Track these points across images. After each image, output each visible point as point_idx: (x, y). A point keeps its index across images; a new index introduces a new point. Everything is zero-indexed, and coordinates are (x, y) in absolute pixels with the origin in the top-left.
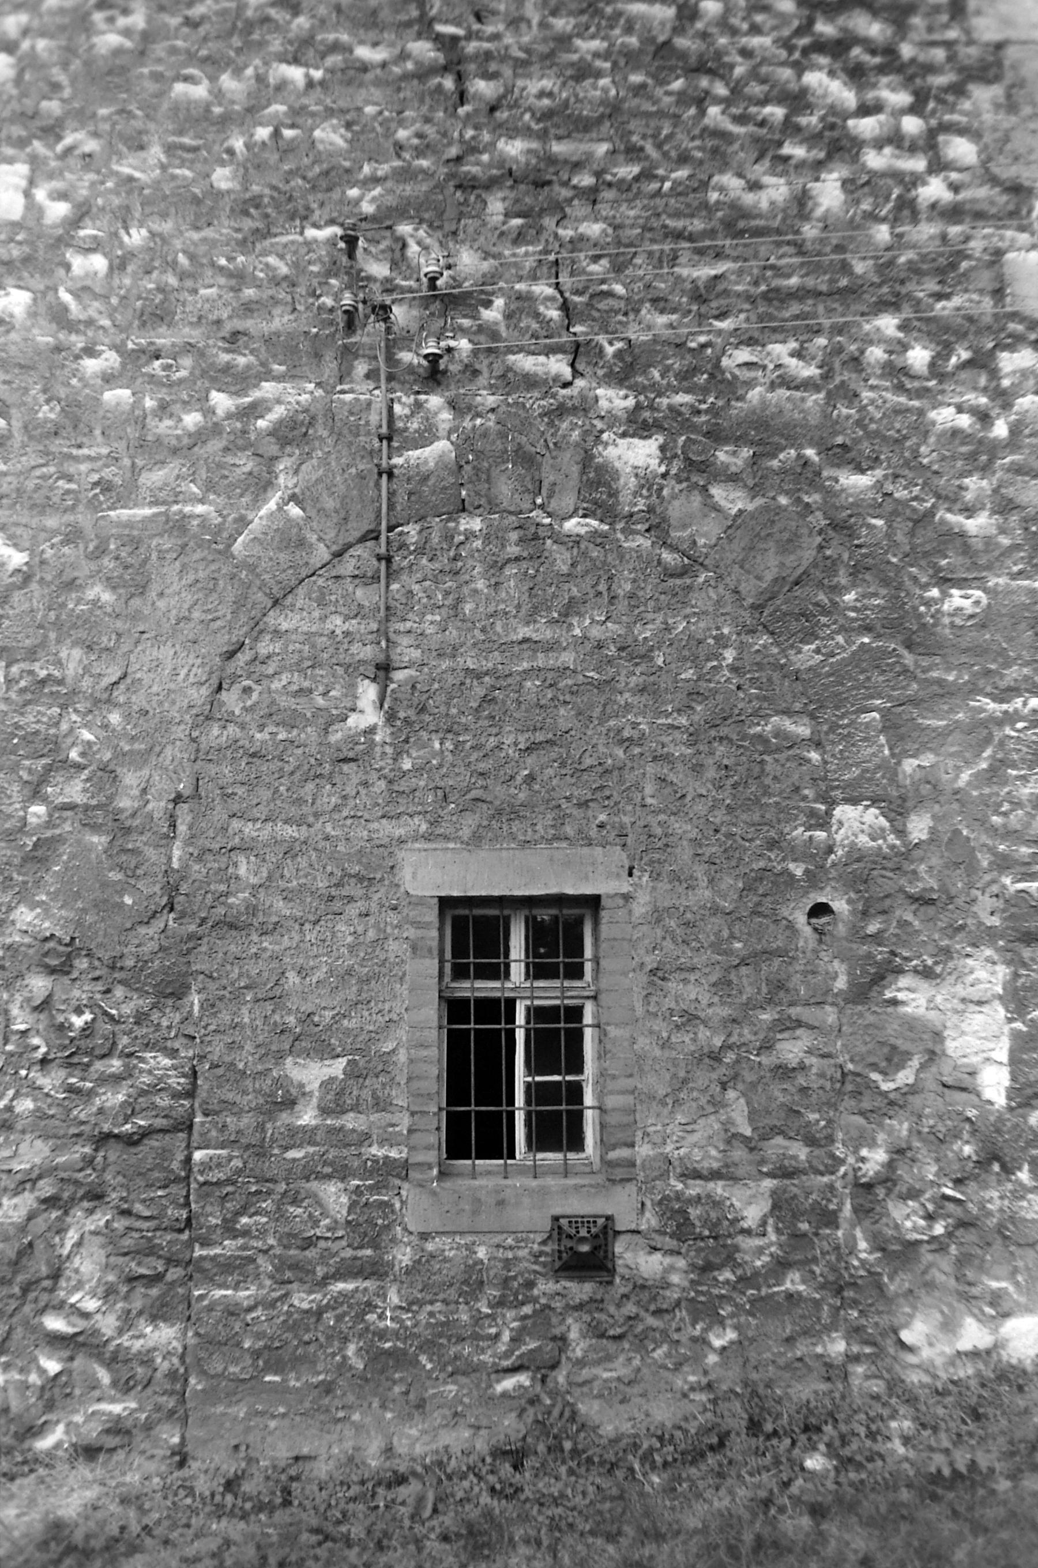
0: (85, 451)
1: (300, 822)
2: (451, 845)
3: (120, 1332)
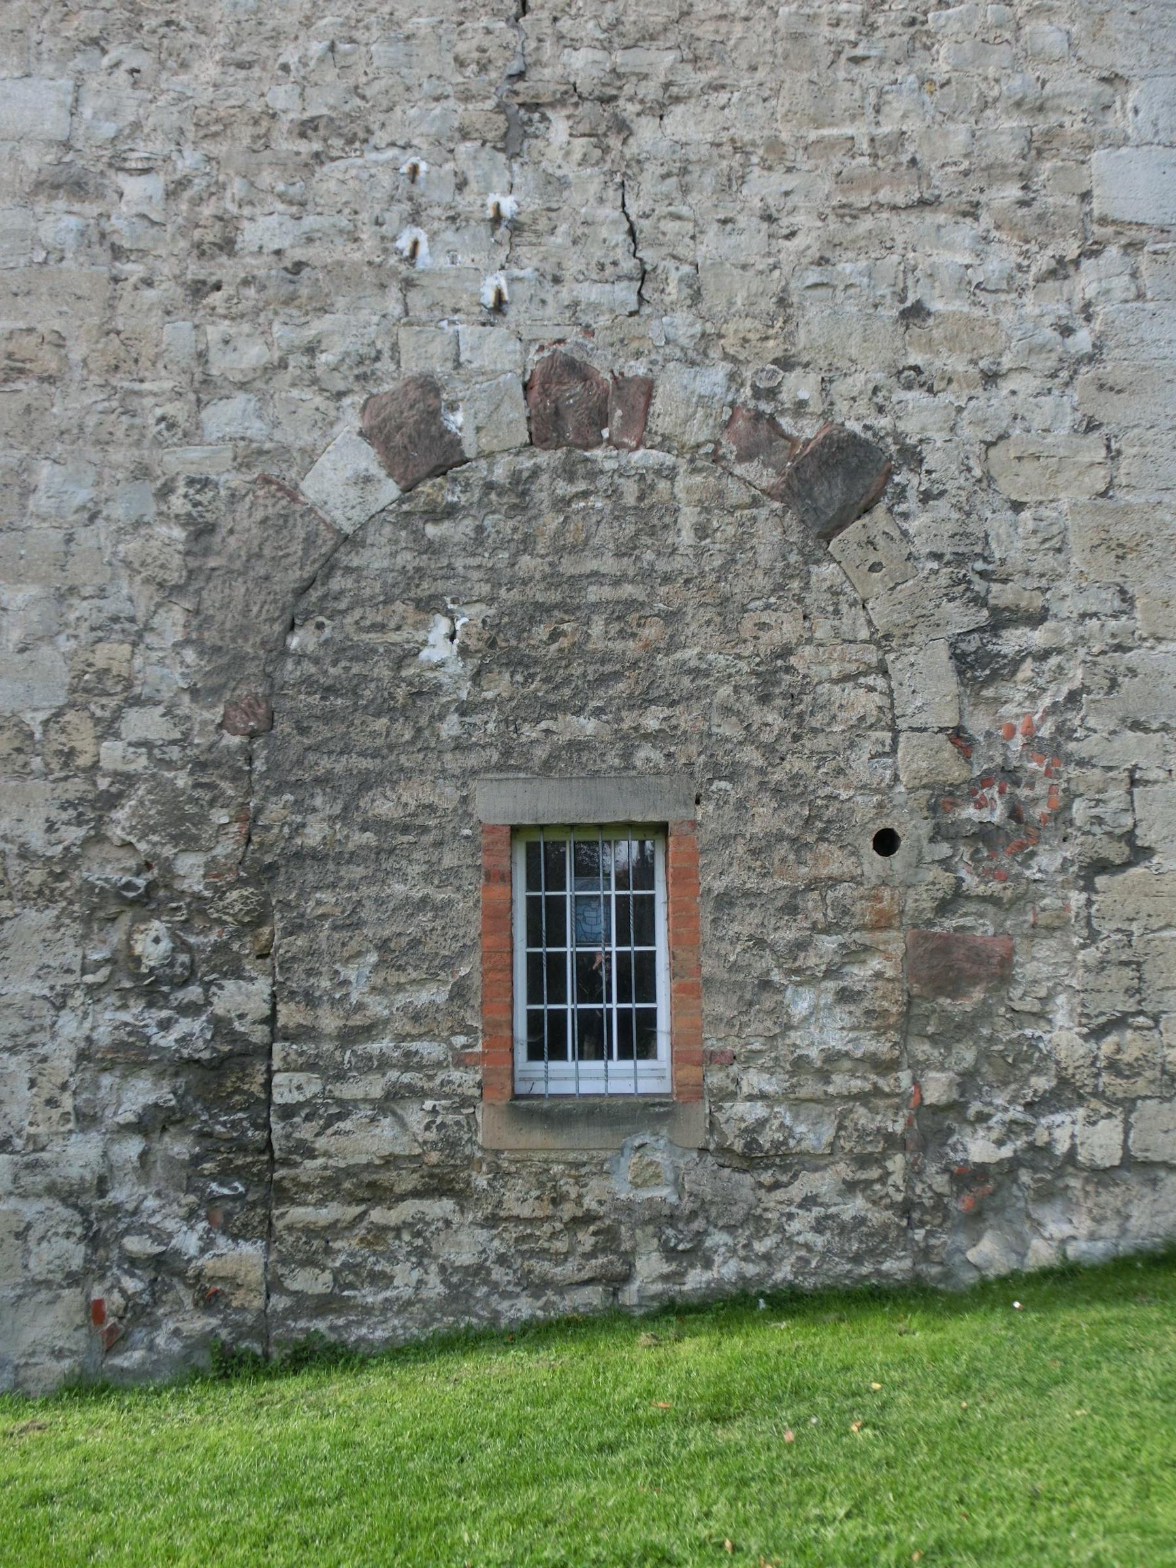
0: (147, 386)
1: (376, 754)
2: (522, 775)
3: (203, 1251)
